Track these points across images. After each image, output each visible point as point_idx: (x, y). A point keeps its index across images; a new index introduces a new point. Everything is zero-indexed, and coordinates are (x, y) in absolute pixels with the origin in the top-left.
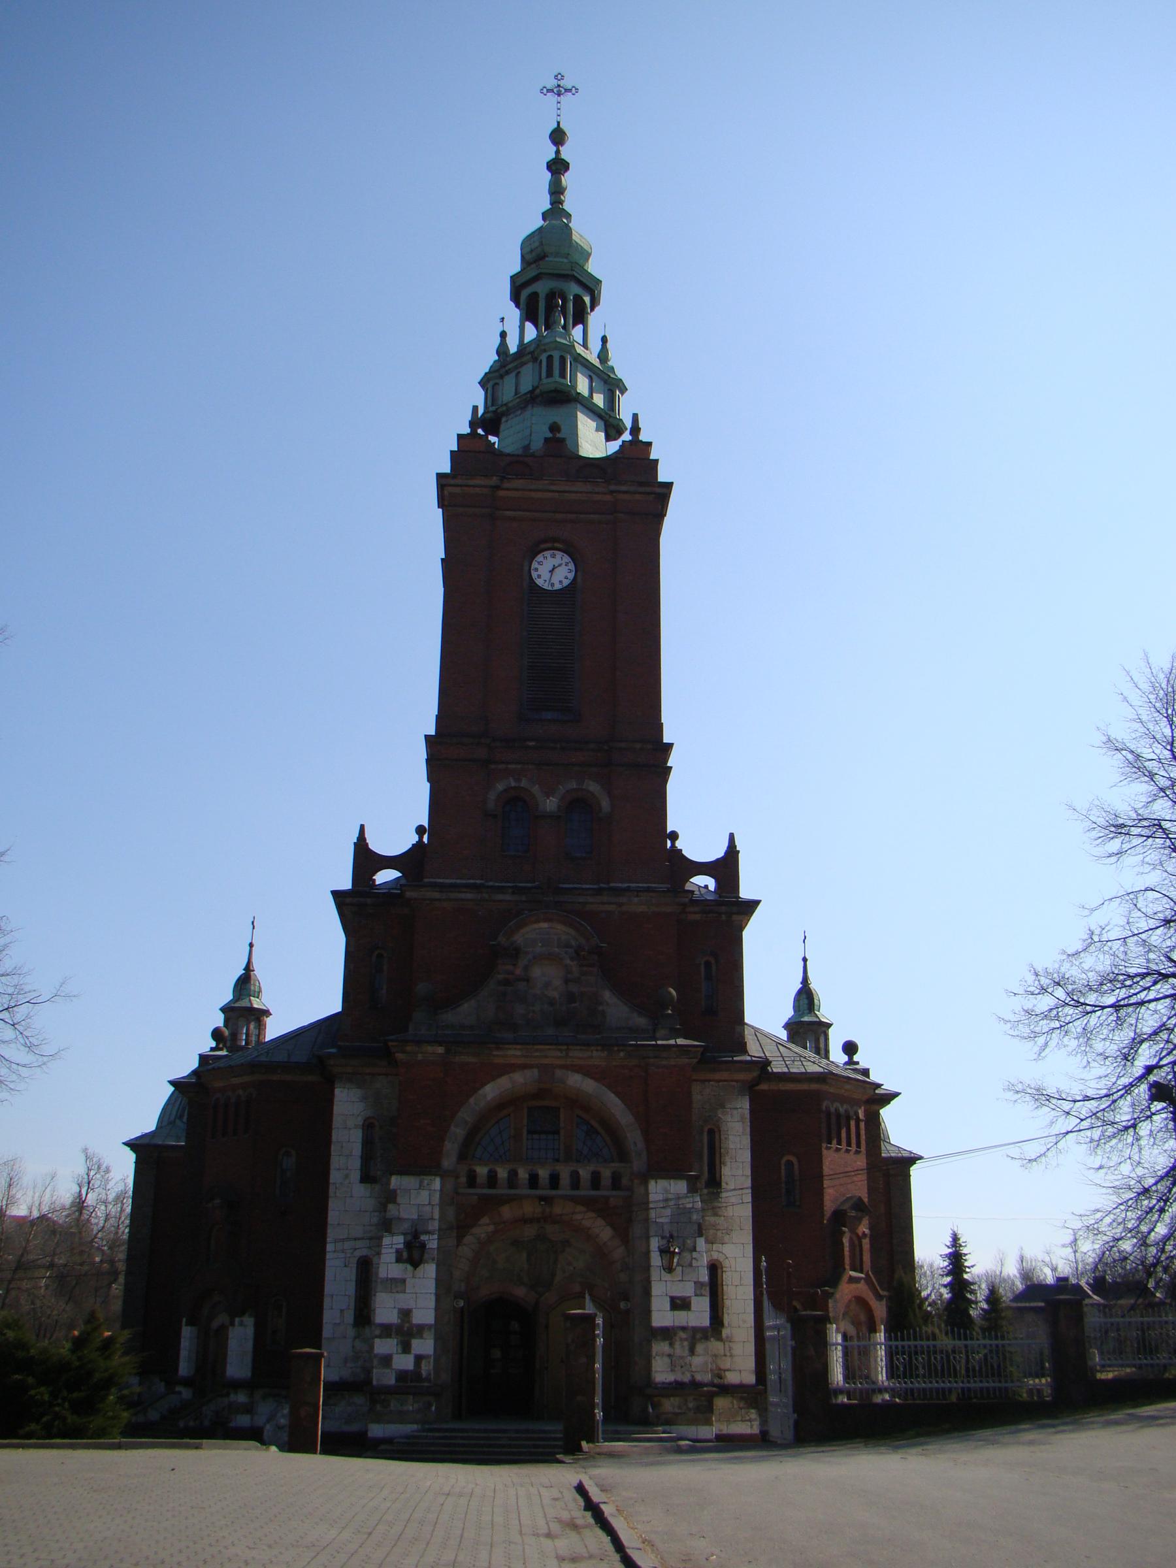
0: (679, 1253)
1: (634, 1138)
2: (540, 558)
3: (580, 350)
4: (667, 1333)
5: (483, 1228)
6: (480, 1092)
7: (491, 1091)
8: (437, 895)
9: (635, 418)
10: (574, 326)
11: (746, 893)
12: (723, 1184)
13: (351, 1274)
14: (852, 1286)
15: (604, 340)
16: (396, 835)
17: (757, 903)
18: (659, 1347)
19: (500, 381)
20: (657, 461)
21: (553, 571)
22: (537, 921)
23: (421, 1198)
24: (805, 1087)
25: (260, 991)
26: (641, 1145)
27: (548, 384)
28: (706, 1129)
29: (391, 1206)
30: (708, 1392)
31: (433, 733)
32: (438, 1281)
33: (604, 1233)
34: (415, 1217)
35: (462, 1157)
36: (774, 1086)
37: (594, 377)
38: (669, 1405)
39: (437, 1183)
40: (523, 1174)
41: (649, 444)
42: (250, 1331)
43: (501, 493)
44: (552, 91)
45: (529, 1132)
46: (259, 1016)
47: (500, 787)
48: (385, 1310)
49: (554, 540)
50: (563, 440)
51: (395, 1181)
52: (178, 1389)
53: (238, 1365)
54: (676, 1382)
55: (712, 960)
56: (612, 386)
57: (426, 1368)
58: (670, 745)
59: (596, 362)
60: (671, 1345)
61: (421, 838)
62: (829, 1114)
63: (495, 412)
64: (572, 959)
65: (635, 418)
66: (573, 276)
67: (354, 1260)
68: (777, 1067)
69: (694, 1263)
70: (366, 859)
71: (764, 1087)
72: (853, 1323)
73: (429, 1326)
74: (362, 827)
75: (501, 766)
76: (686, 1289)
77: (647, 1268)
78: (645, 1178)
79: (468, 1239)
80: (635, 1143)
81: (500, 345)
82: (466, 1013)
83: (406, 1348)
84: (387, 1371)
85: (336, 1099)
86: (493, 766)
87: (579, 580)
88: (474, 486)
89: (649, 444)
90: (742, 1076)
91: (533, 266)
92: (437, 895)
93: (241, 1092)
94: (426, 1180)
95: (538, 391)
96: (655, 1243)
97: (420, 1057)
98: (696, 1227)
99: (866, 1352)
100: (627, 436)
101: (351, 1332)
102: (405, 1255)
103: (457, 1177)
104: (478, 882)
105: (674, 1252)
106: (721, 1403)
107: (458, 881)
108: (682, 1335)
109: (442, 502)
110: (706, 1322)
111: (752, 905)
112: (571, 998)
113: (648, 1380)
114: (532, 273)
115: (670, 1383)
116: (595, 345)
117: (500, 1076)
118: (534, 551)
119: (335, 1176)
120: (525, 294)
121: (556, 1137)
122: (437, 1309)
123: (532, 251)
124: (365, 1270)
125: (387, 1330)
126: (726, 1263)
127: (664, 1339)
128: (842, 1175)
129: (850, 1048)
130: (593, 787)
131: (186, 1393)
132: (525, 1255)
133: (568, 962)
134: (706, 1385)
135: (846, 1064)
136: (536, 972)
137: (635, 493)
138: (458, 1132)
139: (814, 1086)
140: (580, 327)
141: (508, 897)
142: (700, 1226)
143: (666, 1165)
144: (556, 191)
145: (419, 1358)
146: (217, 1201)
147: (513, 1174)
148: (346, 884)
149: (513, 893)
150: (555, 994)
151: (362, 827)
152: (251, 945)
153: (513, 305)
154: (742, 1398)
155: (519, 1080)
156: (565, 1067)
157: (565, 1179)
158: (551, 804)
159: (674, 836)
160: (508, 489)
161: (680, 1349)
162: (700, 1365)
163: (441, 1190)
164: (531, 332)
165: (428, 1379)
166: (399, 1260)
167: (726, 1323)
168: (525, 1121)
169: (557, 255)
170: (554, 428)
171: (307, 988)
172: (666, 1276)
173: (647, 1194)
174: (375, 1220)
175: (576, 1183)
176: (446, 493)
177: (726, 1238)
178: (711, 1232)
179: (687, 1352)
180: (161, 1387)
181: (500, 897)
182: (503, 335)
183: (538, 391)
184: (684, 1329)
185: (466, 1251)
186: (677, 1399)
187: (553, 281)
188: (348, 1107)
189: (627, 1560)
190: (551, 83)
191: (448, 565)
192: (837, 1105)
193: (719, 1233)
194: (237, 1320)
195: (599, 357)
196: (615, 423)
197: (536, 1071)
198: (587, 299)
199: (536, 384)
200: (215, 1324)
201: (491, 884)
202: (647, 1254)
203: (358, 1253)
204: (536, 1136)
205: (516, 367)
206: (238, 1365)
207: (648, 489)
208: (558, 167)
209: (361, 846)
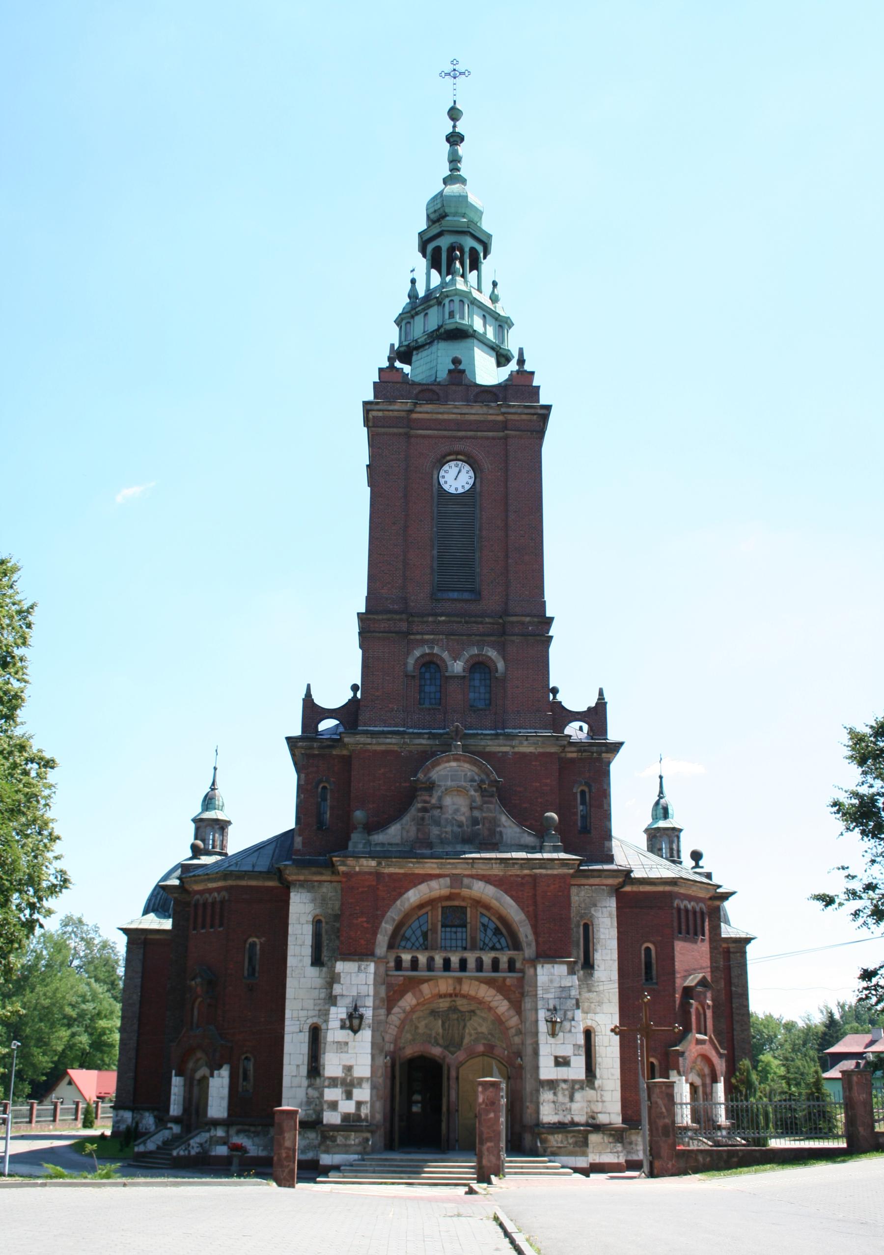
0: (561, 1022)
1: (525, 932)
2: (446, 467)
3: (475, 294)
4: (552, 1084)
5: (409, 1000)
6: (405, 896)
7: (413, 896)
8: (369, 740)
9: (521, 352)
10: (470, 271)
11: (612, 736)
12: (596, 967)
13: (305, 1037)
14: (698, 1045)
15: (495, 284)
16: (335, 694)
17: (621, 744)
18: (546, 1096)
19: (412, 321)
20: (538, 387)
21: (456, 478)
22: (448, 761)
23: (358, 979)
24: (660, 888)
25: (223, 806)
26: (531, 937)
27: (450, 325)
28: (582, 923)
29: (335, 986)
30: (584, 1130)
31: (363, 611)
32: (373, 1044)
33: (502, 1006)
34: (355, 994)
35: (391, 946)
36: (635, 888)
37: (487, 316)
38: (555, 1140)
39: (372, 967)
40: (439, 960)
41: (532, 373)
42: (226, 1081)
43: (414, 416)
44: (449, 74)
45: (442, 926)
46: (222, 826)
47: (417, 653)
48: (332, 1066)
49: (458, 453)
50: (463, 371)
51: (340, 966)
52: (169, 1125)
53: (217, 1103)
54: (560, 1123)
55: (587, 790)
56: (503, 324)
57: (365, 1111)
58: (552, 619)
59: (488, 303)
60: (555, 1094)
61: (355, 694)
62: (679, 910)
63: (408, 346)
64: (476, 791)
65: (521, 352)
66: (469, 232)
67: (306, 1028)
68: (636, 874)
69: (573, 1030)
70: (312, 712)
71: (628, 889)
72: (699, 1075)
73: (368, 1079)
74: (309, 686)
75: (419, 637)
76: (566, 1051)
77: (536, 1034)
78: (533, 962)
79: (396, 1010)
80: (526, 936)
81: (411, 290)
82: (394, 833)
83: (349, 1096)
84: (334, 1113)
85: (291, 901)
86: (412, 637)
87: (478, 485)
88: (392, 411)
89: (532, 373)
90: (610, 881)
91: (437, 224)
92: (369, 740)
93: (216, 894)
94: (364, 964)
95: (442, 330)
96: (542, 1014)
97: (357, 869)
98: (574, 1002)
99: (709, 1095)
100: (513, 366)
101: (305, 1083)
102: (347, 1023)
103: (388, 963)
104: (402, 729)
105: (556, 1022)
106: (594, 1138)
107: (385, 729)
108: (564, 1086)
109: (367, 422)
110: (582, 1076)
111: (616, 747)
112: (475, 821)
113: (538, 1124)
114: (435, 230)
115: (554, 1124)
116: (487, 288)
117: (420, 883)
118: (441, 462)
119: (291, 961)
120: (430, 247)
121: (464, 929)
122: (372, 1066)
123: (435, 211)
124: (316, 1036)
125: (334, 1082)
126: (598, 1029)
127: (550, 1089)
128: (691, 961)
129: (696, 856)
130: (492, 653)
131: (176, 1129)
132: (440, 1022)
133: (473, 793)
134: (582, 1125)
135: (693, 868)
136: (448, 801)
137: (520, 414)
138: (387, 927)
139: (668, 888)
140: (475, 272)
141: (424, 742)
142: (577, 1001)
143: (549, 954)
144: (454, 160)
145: (359, 1104)
146: (199, 980)
147: (431, 960)
148: (297, 731)
149: (429, 738)
150: (463, 819)
151: (309, 686)
152: (215, 769)
153: (420, 255)
154: (611, 1135)
155: (436, 888)
156: (471, 876)
157: (471, 964)
158: (458, 667)
159: (555, 691)
160: (420, 413)
161: (562, 1098)
162: (578, 1112)
163: (375, 973)
164: (436, 279)
165: (366, 1120)
166: (343, 1027)
167: (598, 1075)
168: (440, 918)
169: (455, 214)
170: (456, 361)
171: (265, 808)
172: (551, 1040)
173: (536, 975)
174: (323, 996)
175: (480, 966)
176: (370, 416)
177: (598, 1009)
178: (586, 1004)
179: (567, 1100)
180: (149, 1120)
181: (417, 741)
182: (413, 281)
183: (442, 330)
184: (565, 1081)
185: (396, 1017)
186: (560, 1136)
187: (452, 240)
188: (301, 910)
189: (517, 1248)
190: (448, 68)
191: (374, 472)
192: (686, 902)
193: (592, 1005)
194: (216, 1072)
195: (490, 298)
196: (504, 352)
197: (448, 879)
198: (480, 248)
199: (440, 324)
200: (198, 1075)
201: (411, 730)
202: (537, 1021)
203: (310, 1021)
204: (448, 929)
205: (424, 310)
206: (217, 1103)
207: (532, 411)
208: (455, 139)
209: (309, 703)
